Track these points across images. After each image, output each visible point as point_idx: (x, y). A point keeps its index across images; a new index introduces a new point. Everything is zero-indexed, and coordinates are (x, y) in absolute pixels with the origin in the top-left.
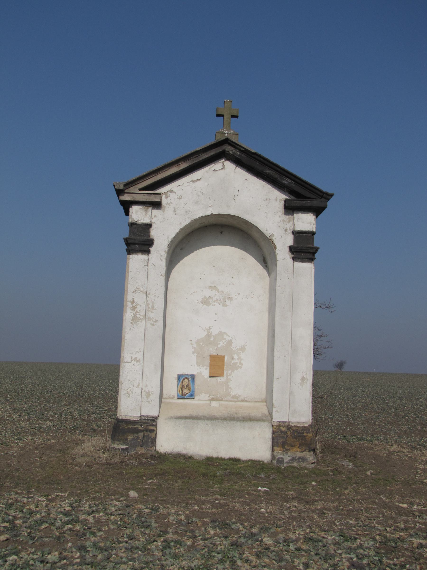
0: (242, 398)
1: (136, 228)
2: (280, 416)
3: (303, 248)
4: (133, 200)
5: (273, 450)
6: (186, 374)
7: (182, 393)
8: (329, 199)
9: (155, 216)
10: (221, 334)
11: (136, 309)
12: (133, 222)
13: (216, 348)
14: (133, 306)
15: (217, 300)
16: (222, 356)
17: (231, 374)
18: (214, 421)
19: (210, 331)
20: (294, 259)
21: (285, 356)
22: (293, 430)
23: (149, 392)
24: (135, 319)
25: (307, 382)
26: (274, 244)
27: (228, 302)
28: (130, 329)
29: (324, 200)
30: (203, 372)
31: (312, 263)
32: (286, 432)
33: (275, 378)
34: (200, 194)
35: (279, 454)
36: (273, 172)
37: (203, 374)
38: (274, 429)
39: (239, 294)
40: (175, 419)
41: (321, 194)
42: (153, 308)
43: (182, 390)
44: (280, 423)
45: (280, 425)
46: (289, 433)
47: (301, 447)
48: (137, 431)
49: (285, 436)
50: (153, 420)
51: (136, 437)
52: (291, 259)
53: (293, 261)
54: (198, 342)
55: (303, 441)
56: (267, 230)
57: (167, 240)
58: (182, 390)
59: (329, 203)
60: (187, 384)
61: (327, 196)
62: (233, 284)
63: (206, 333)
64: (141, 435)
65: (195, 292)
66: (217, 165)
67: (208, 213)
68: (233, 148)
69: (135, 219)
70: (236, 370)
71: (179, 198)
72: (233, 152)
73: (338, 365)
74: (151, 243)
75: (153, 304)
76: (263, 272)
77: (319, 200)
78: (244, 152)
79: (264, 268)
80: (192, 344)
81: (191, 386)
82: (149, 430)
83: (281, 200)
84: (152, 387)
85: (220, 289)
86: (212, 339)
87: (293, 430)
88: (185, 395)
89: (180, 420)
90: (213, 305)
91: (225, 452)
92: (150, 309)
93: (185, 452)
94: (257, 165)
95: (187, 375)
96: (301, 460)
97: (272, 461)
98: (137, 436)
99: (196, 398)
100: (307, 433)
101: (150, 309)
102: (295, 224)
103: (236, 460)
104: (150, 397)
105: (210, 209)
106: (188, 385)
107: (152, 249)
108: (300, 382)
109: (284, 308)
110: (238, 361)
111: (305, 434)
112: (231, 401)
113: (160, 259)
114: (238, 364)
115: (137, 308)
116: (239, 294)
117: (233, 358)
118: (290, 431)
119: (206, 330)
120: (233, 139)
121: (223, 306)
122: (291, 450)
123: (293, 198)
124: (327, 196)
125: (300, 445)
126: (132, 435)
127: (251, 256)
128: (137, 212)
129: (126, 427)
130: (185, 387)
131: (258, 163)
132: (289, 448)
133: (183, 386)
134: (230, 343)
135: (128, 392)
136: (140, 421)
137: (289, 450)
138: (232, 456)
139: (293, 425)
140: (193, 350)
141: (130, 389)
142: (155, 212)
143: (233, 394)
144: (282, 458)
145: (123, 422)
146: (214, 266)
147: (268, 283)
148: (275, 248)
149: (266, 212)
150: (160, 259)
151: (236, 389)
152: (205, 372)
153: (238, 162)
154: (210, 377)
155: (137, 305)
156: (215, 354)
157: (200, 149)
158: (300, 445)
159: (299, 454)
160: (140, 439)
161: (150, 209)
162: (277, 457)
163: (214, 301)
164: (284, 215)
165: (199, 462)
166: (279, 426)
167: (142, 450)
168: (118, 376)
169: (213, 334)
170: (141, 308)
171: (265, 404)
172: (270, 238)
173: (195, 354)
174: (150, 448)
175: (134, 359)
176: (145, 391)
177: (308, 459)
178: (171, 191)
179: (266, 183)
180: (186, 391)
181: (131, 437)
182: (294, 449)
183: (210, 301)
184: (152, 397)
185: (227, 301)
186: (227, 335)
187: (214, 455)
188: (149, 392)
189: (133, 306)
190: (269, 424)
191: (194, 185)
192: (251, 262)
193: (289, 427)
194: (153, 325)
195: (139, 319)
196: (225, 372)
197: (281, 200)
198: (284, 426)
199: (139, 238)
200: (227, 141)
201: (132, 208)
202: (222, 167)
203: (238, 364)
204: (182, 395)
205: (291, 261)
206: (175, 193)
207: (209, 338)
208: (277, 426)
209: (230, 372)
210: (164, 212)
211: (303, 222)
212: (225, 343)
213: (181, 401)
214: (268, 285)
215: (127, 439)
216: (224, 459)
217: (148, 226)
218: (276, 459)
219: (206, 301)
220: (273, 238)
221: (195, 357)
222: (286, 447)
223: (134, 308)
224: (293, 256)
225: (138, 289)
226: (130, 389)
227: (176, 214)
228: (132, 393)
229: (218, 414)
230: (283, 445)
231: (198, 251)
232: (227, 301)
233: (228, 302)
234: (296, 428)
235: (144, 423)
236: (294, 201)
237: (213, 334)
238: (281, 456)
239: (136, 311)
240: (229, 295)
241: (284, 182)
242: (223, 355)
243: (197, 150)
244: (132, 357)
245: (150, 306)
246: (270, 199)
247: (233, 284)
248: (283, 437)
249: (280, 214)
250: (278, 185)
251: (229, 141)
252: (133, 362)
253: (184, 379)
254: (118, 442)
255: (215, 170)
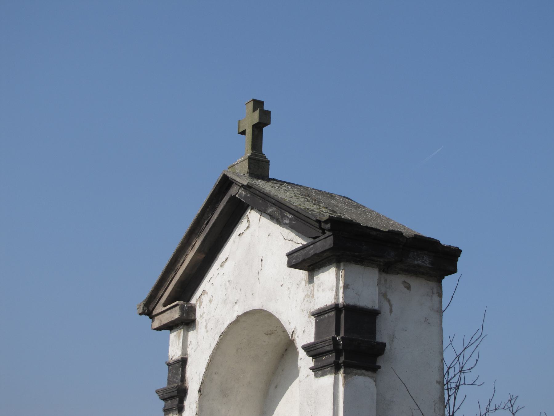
20: (316, 376)
71: (210, 302)
105: (237, 307)
153: (262, 211)
178: (204, 292)
249: (303, 283)
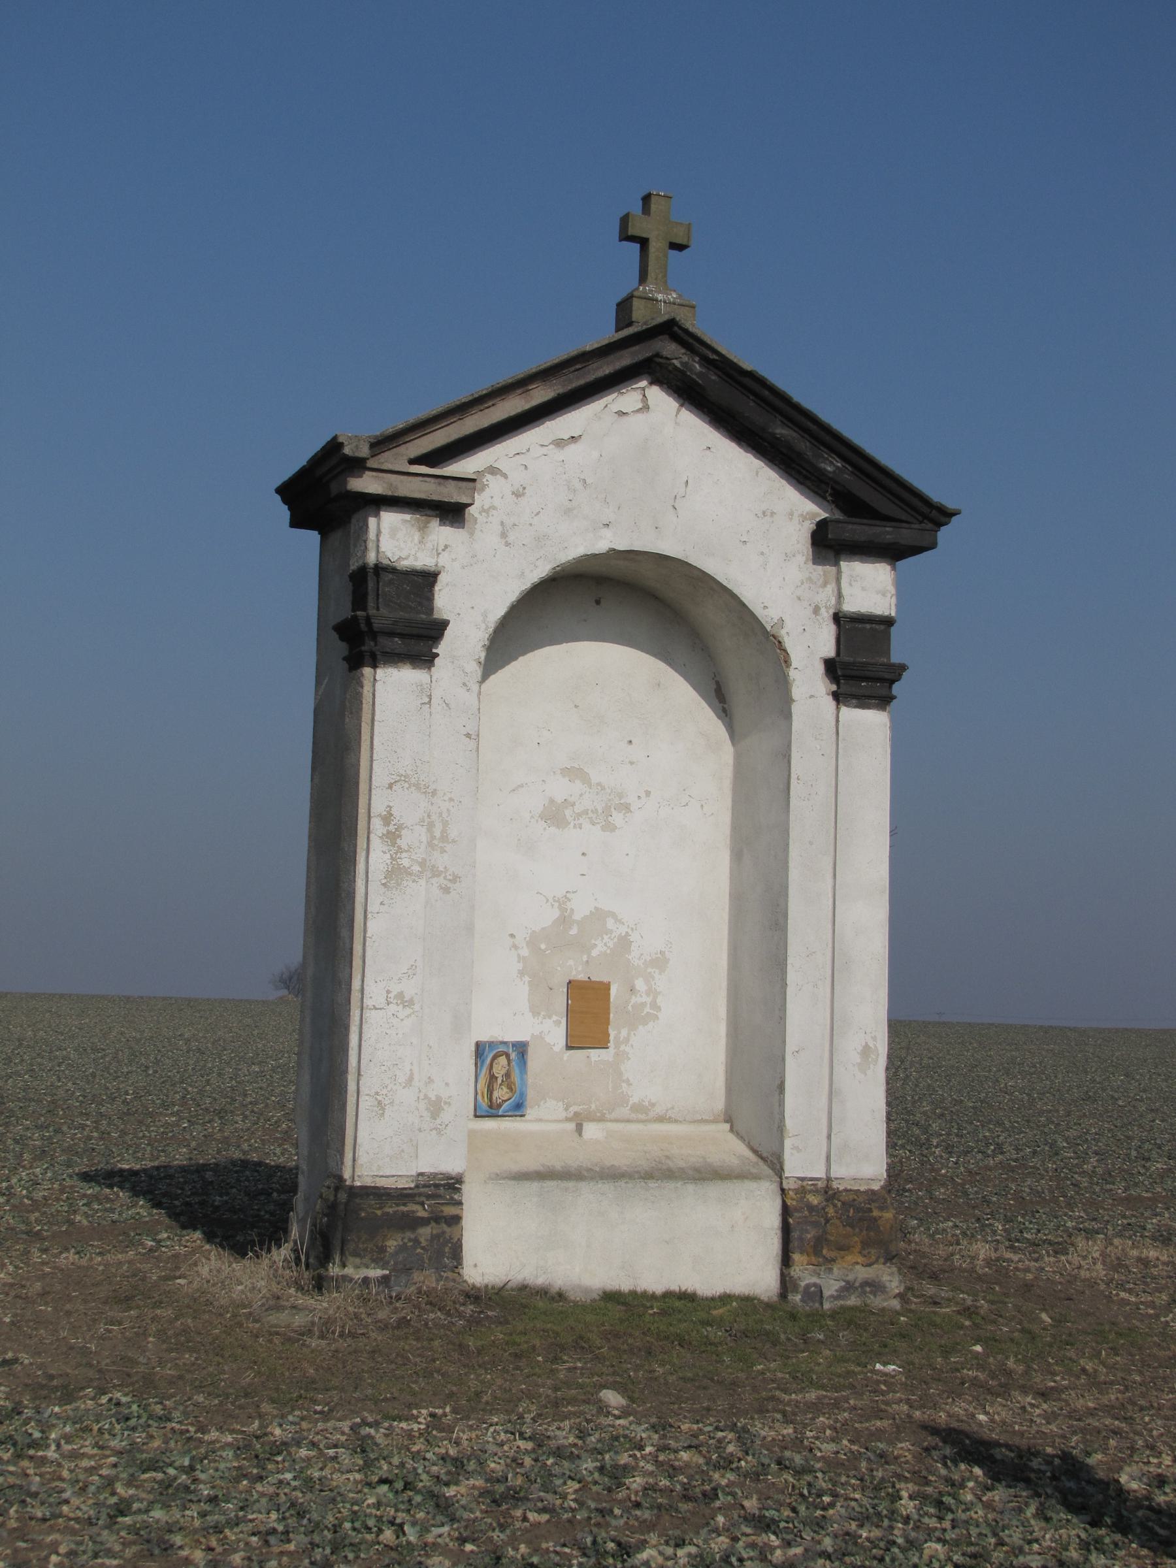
0: (658, 1110)
1: (391, 582)
2: (802, 1164)
3: (863, 666)
4: (390, 493)
5: (786, 1260)
6: (500, 1039)
7: (491, 1100)
8: (939, 525)
9: (446, 547)
10: (599, 916)
11: (398, 841)
12: (385, 562)
13: (585, 958)
14: (389, 832)
15: (586, 812)
16: (601, 983)
17: (627, 1040)
18: (622, 1183)
19: (569, 905)
21: (815, 986)
22: (843, 1203)
23: (439, 1098)
24: (396, 873)
25: (876, 1061)
26: (785, 650)
27: (617, 818)
28: (382, 903)
29: (930, 526)
30: (548, 1032)
31: (884, 709)
32: (824, 1209)
33: (790, 1048)
34: (578, 485)
35: (804, 1272)
36: (794, 434)
37: (547, 1039)
38: (789, 1202)
39: (648, 793)
40: (510, 1182)
41: (926, 510)
42: (444, 838)
43: (490, 1091)
44: (805, 1183)
45: (805, 1187)
46: (831, 1211)
47: (865, 1252)
48: (413, 1223)
49: (814, 1221)
50: (451, 1185)
51: (410, 1240)
52: (831, 698)
53: (834, 703)
54: (533, 941)
55: (872, 1234)
56: (765, 607)
57: (483, 626)
58: (490, 1091)
59: (944, 534)
60: (503, 1072)
61: (939, 516)
62: (632, 763)
63: (556, 913)
64: (425, 1232)
65: (522, 786)
66: (627, 399)
67: (602, 546)
68: (683, 351)
69: (389, 555)
70: (641, 1027)
71: (518, 494)
72: (681, 363)
73: (290, 979)
74: (436, 630)
75: (445, 824)
76: (718, 729)
77: (917, 526)
78: (717, 367)
79: (719, 717)
80: (515, 947)
81: (516, 1076)
82: (444, 1217)
83: (804, 518)
84: (447, 1084)
85: (595, 778)
86: (574, 931)
87: (843, 1203)
88: (500, 1106)
89: (527, 1184)
90: (575, 826)
91: (655, 1275)
92: (436, 842)
93: (540, 1281)
94: (749, 409)
95: (505, 1043)
96: (868, 1289)
97: (783, 1295)
98: (412, 1236)
99: (531, 1113)
100: (881, 1209)
101: (436, 842)
102: (844, 592)
103: (688, 1297)
104: (441, 1115)
105: (608, 533)
106: (508, 1075)
107: (442, 649)
108: (859, 1061)
109: (811, 843)
110: (649, 1000)
111: (876, 1213)
112: (628, 1121)
113: (464, 684)
114: (647, 1009)
115: (400, 836)
116: (648, 793)
117: (632, 990)
118: (835, 1206)
119: (556, 904)
120: (697, 325)
121: (604, 829)
122: (839, 1260)
123: (838, 515)
124: (939, 516)
125: (866, 1244)
126: (399, 1236)
127: (682, 679)
128: (394, 532)
129: (379, 1212)
130: (499, 1081)
131: (752, 404)
132: (833, 1254)
133: (493, 1078)
134: (624, 943)
135: (380, 1103)
136: (416, 1191)
137: (833, 1260)
138: (674, 1287)
139: (841, 1188)
140: (520, 966)
141: (384, 1091)
142: (441, 533)
143: (634, 1100)
144: (815, 1285)
145: (368, 1195)
146: (576, 706)
147: (731, 761)
148: (787, 662)
149: (762, 553)
150: (464, 684)
151: (644, 1087)
152: (554, 1032)
153: (690, 394)
154: (569, 1047)
155: (400, 828)
156: (582, 977)
157: (596, 346)
158: (866, 1244)
159: (862, 1273)
160: (423, 1248)
161: (435, 523)
162: (803, 1284)
163: (579, 815)
164: (810, 563)
165: (581, 1307)
166: (802, 1191)
167: (426, 1279)
168: (343, 1048)
169: (577, 917)
170: (414, 837)
171: (727, 1126)
172: (774, 632)
173: (527, 979)
174: (450, 1274)
175: (396, 997)
176: (426, 1097)
177: (888, 1284)
178: (493, 470)
179: (762, 464)
180: (500, 1093)
181: (395, 1243)
182: (849, 1258)
183: (568, 812)
184: (446, 1116)
185: (614, 813)
186: (618, 921)
187: (625, 1286)
188: (439, 1098)
189: (389, 832)
190: (775, 1187)
191: (559, 455)
192: (679, 696)
193: (829, 1192)
194: (446, 890)
195: (407, 872)
196: (612, 1033)
197: (804, 518)
198: (816, 1191)
199: (407, 616)
200: (670, 329)
201: (377, 515)
202: (640, 405)
203: (647, 1009)
204: (491, 1107)
205: (830, 703)
206: (505, 476)
207: (566, 930)
208: (796, 1191)
209: (624, 1032)
210: (472, 534)
211: (863, 589)
212: (611, 944)
213: (489, 1124)
214: (731, 768)
215: (382, 1249)
216: (653, 1297)
217: (428, 579)
218: (801, 1289)
219: (554, 815)
220: (783, 632)
221: (526, 988)
222: (825, 1252)
223: (392, 837)
224: (834, 687)
225: (405, 778)
226: (384, 1091)
227: (507, 544)
228: (392, 1103)
229: (621, 1162)
230: (816, 1248)
231: (530, 655)
232: (614, 813)
233: (617, 818)
234: (851, 1197)
235: (429, 1197)
236: (850, 526)
237: (577, 917)
238: (814, 1280)
239: (399, 847)
240: (621, 796)
241: (822, 465)
242: (605, 980)
243: (588, 348)
244: (388, 992)
245: (437, 834)
246: (773, 514)
247: (632, 763)
248: (815, 1224)
249: (801, 559)
250: (800, 473)
251: (676, 329)
252: (393, 1008)
253: (495, 1058)
254: (358, 1261)
255: (621, 414)
